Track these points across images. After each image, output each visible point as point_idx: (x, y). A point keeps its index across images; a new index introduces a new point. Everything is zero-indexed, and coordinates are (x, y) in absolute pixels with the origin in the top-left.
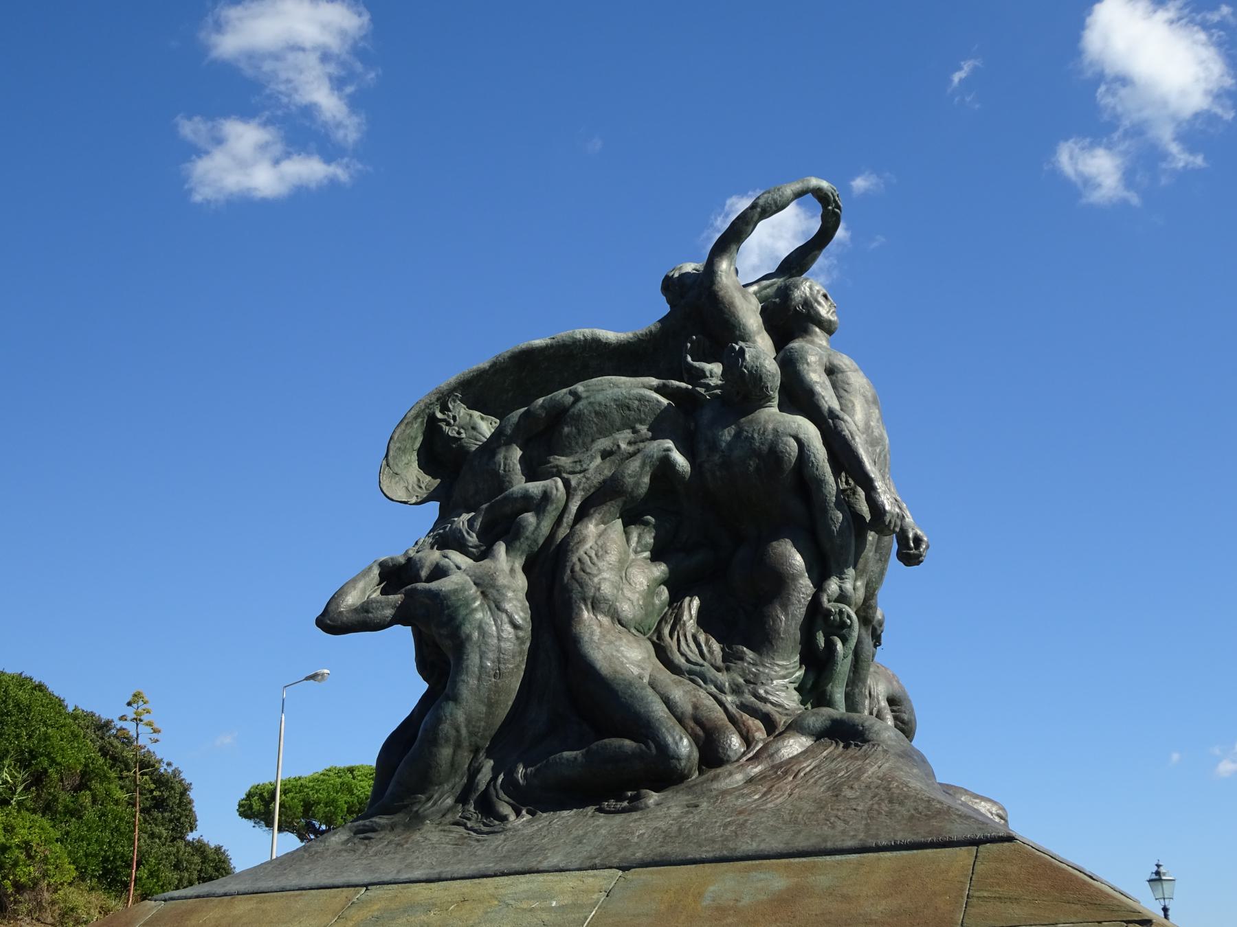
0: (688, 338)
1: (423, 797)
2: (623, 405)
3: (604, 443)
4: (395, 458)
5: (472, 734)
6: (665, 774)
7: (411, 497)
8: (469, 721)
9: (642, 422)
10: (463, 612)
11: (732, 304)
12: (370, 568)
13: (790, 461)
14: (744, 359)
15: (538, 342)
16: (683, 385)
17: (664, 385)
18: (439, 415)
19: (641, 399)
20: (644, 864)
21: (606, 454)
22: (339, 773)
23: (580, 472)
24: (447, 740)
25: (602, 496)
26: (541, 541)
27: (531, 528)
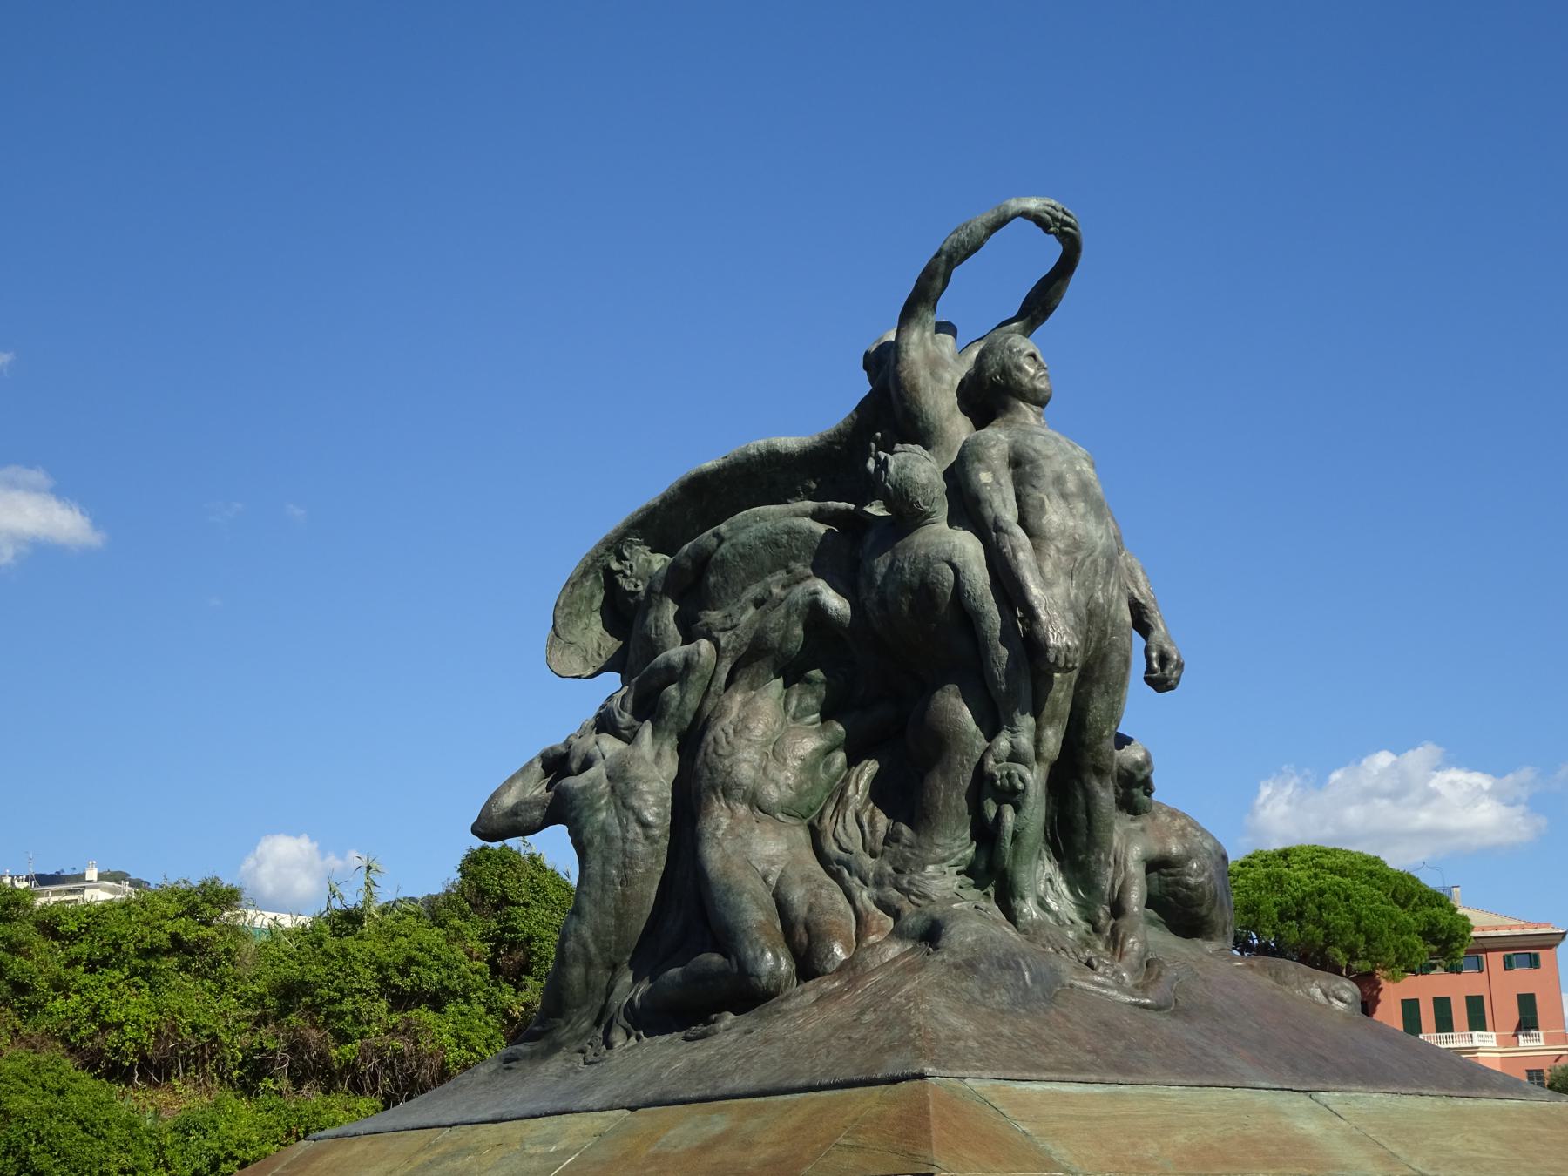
0: (872, 438)
1: (562, 1022)
2: (771, 542)
3: (755, 590)
4: (565, 625)
5: (602, 950)
6: (748, 995)
7: (586, 669)
8: (596, 936)
9: (796, 559)
10: (586, 813)
11: (914, 387)
12: (531, 762)
13: (945, 594)
14: (887, 472)
15: (709, 464)
16: (843, 505)
17: (820, 509)
18: (615, 566)
19: (790, 532)
20: (648, 1105)
21: (758, 603)
22: (1267, 859)
23: (732, 628)
24: (575, 959)
25: (753, 659)
26: (689, 717)
27: (674, 704)
